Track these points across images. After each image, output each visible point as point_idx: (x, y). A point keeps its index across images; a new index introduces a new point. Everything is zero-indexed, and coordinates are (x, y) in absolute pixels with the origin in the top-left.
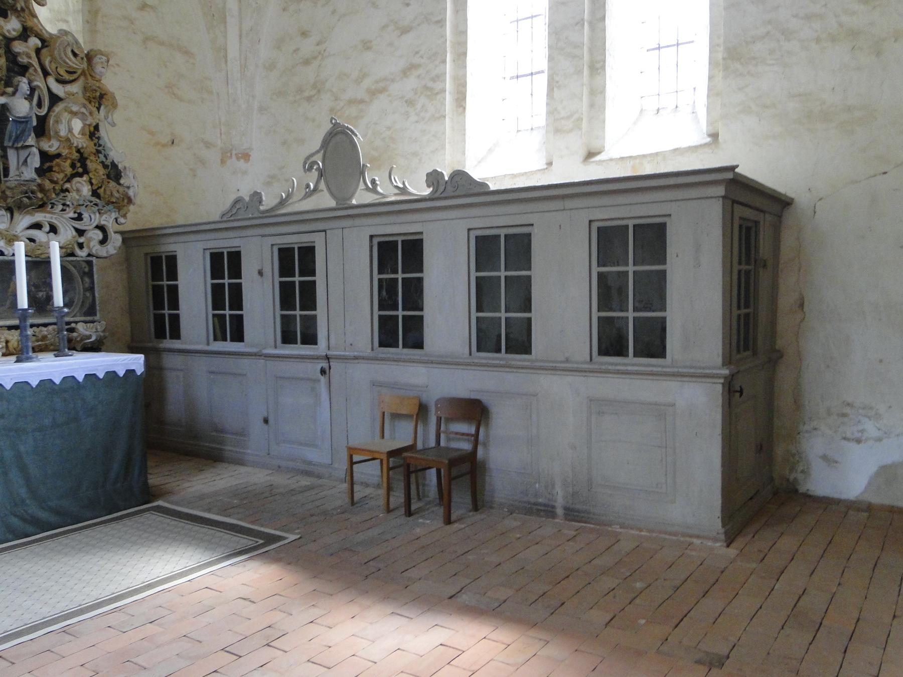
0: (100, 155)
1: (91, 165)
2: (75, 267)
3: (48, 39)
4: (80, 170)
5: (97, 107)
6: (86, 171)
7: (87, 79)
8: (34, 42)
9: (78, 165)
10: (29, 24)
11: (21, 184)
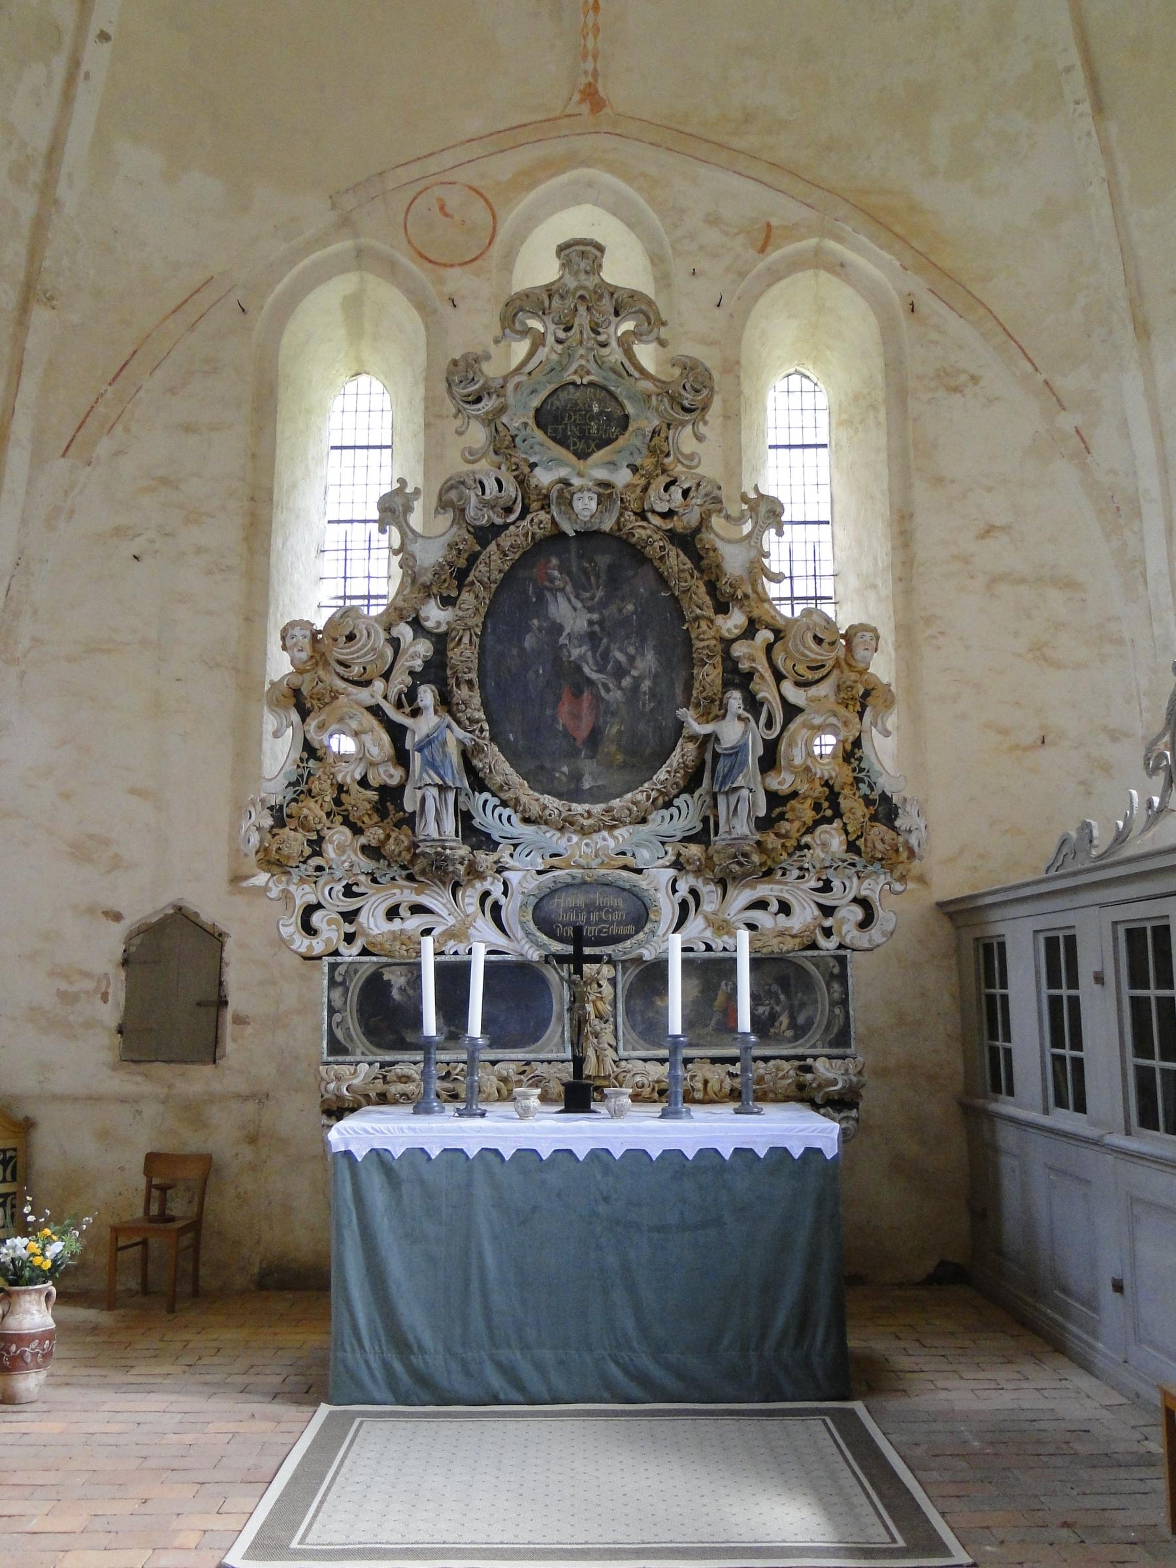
0: (861, 785)
1: (844, 804)
2: (817, 966)
3: (783, 628)
4: (829, 813)
5: (858, 712)
6: (838, 814)
7: (842, 672)
8: (765, 635)
9: (826, 805)
10: (756, 614)
11: (729, 845)
